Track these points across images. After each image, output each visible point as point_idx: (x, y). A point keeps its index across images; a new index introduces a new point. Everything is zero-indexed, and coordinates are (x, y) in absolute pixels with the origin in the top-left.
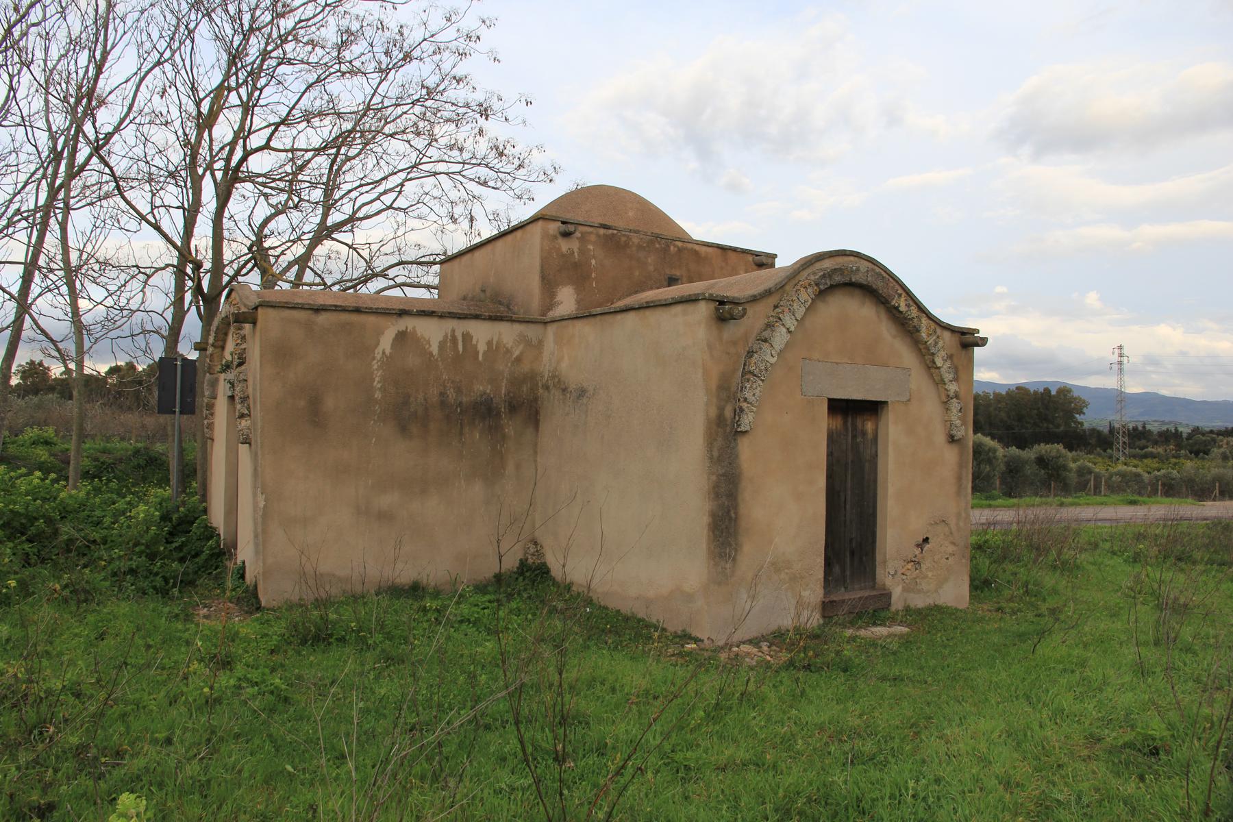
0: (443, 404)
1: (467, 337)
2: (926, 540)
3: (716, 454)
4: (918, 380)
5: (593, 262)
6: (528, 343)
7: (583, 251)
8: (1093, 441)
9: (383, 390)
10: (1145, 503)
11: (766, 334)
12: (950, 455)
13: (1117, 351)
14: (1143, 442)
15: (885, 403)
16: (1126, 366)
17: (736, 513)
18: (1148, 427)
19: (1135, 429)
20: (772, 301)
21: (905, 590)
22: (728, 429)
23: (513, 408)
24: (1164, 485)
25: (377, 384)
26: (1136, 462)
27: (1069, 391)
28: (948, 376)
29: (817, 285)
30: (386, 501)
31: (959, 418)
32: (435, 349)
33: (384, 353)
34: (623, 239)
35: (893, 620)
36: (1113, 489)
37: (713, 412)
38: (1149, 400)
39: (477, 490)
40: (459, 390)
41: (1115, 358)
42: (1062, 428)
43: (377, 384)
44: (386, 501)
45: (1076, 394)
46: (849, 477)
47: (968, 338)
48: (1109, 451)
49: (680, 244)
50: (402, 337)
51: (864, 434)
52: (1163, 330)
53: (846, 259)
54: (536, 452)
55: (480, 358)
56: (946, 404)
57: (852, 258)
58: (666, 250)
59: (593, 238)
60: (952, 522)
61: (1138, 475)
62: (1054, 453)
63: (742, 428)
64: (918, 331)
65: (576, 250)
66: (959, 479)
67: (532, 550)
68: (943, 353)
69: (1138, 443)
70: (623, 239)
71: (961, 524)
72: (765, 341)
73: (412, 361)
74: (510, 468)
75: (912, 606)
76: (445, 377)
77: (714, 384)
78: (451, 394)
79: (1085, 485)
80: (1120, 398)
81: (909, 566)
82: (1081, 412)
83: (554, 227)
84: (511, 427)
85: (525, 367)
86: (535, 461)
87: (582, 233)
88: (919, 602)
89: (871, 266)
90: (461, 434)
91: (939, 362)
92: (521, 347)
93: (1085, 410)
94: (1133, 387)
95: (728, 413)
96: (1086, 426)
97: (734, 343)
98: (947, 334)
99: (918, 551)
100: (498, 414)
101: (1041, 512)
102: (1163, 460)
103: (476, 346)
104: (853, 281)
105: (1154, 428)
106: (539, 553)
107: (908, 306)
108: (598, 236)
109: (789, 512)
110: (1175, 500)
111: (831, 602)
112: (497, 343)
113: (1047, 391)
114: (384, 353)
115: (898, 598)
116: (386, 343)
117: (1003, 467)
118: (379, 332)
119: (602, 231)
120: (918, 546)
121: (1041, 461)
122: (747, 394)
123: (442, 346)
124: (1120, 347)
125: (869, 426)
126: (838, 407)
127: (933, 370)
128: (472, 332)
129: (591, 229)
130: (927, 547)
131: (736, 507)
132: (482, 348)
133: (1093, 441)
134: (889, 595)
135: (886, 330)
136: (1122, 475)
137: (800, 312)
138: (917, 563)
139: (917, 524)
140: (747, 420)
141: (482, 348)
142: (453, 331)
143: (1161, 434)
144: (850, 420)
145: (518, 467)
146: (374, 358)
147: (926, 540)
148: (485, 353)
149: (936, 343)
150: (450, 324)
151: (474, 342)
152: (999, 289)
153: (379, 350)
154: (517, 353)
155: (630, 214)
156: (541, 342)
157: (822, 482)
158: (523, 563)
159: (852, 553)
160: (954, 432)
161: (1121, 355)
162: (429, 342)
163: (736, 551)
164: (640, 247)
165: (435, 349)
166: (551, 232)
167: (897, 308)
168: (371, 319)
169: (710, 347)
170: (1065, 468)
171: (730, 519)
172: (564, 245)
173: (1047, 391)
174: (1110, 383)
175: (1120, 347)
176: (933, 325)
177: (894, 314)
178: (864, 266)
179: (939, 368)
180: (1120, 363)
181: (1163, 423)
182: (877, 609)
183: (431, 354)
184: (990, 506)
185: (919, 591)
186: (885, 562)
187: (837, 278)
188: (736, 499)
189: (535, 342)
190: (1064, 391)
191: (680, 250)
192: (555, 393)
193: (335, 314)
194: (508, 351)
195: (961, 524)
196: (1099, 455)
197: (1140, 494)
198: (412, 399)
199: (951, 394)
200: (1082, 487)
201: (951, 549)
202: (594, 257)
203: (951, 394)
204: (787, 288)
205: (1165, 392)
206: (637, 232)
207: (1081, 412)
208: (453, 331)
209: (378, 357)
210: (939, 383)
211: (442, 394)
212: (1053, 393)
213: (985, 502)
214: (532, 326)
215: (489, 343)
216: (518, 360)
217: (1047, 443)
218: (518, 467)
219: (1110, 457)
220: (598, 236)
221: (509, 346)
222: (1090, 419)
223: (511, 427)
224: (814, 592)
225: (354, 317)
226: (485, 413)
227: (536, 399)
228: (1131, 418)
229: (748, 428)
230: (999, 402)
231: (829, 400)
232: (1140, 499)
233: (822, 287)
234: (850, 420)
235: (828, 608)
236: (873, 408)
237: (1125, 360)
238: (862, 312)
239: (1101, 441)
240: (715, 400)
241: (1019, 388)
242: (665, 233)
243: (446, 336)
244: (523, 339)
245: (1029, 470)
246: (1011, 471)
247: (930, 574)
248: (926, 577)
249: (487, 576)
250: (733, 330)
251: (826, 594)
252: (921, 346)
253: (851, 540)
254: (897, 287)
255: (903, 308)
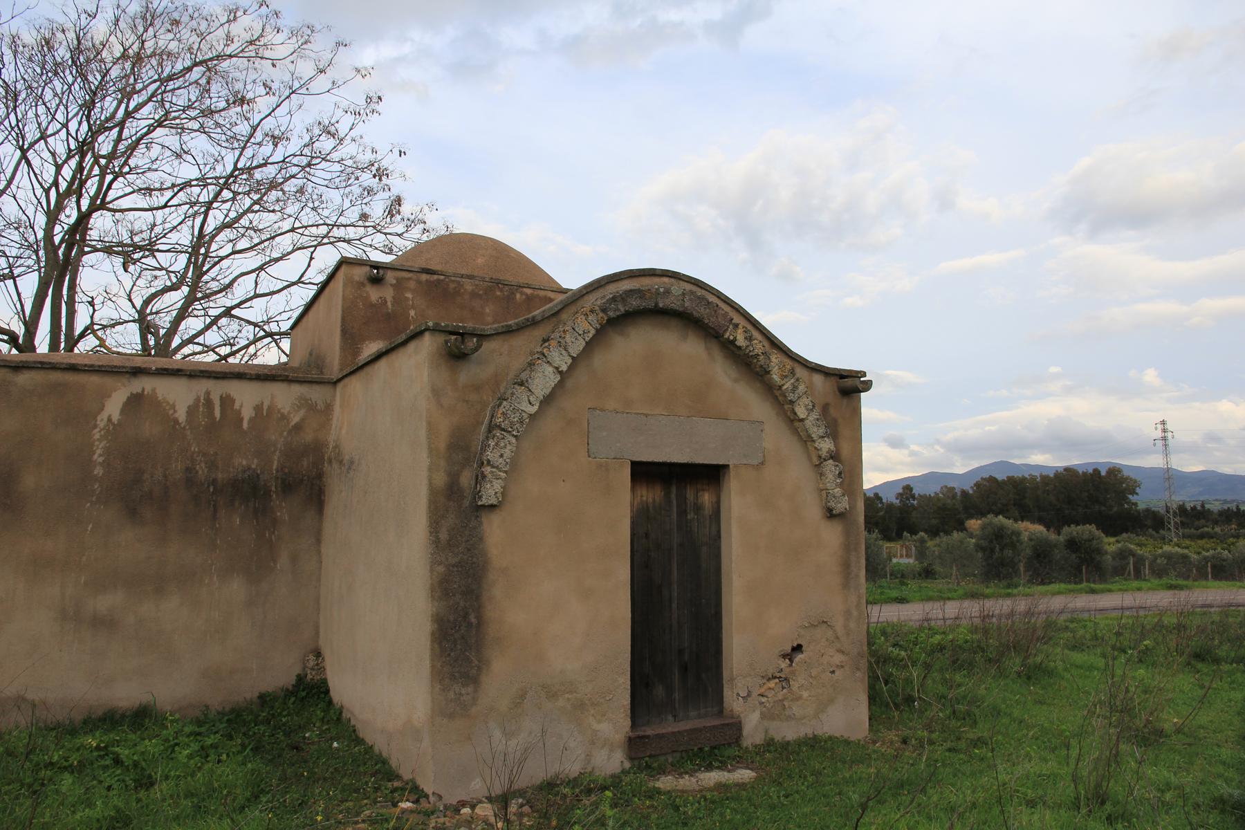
0: (189, 480)
1: (227, 401)
2: (798, 648)
3: (444, 536)
4: (775, 436)
5: (412, 313)
6: (312, 408)
7: (396, 300)
8: (1149, 522)
9: (106, 464)
10: (1187, 587)
11: (524, 376)
12: (832, 535)
13: (1160, 427)
14: (1203, 522)
15: (726, 467)
16: (1170, 441)
17: (479, 618)
18: (1207, 506)
19: (1194, 508)
20: (539, 333)
21: (763, 716)
22: (466, 503)
23: (288, 485)
24: (1213, 567)
25: (98, 457)
26: (1188, 542)
27: (1119, 471)
28: (816, 431)
29: (604, 310)
30: (104, 603)
31: (841, 485)
32: (181, 415)
33: (109, 420)
34: (452, 286)
35: (742, 760)
36: (1159, 573)
37: (441, 479)
38: (1207, 479)
39: (236, 588)
40: (212, 465)
41: (1159, 434)
42: (1115, 509)
43: (98, 457)
44: (104, 603)
45: (1126, 473)
46: (675, 566)
47: (848, 382)
48: (1162, 532)
49: (529, 291)
50: (135, 402)
51: (698, 508)
52: (1225, 406)
53: (657, 280)
54: (319, 541)
55: (245, 425)
56: (818, 467)
57: (666, 280)
58: (510, 298)
59: (412, 285)
60: (839, 623)
61: (1185, 557)
62: (1086, 537)
63: (484, 501)
64: (768, 372)
65: (389, 299)
66: (846, 566)
67: (311, 663)
68: (805, 401)
69: (1196, 523)
70: (452, 286)
71: (852, 625)
72: (521, 384)
73: (149, 429)
74: (283, 561)
75: (778, 738)
76: (194, 448)
77: (442, 445)
78: (202, 470)
79: (1128, 569)
80: (1169, 477)
81: (772, 684)
82: (1134, 493)
83: (360, 273)
84: (283, 509)
85: (308, 436)
86: (319, 552)
87: (398, 279)
88: (788, 732)
89: (688, 287)
90: (214, 517)
91: (801, 412)
92: (302, 413)
93: (1138, 490)
94: (1190, 465)
95: (466, 479)
96: (1141, 506)
97: (477, 388)
98: (818, 379)
99: (784, 664)
100: (268, 493)
101: (1128, 599)
102: (1221, 539)
103: (239, 412)
104: (660, 306)
105: (1215, 507)
106: (320, 668)
107: (750, 339)
108: (419, 282)
109: (570, 612)
110: (1223, 583)
111: (639, 737)
112: (269, 407)
113: (1096, 472)
114: (109, 420)
115: (753, 728)
116: (113, 408)
117: (1029, 552)
118: (105, 395)
119: (424, 277)
120: (784, 656)
121: (1072, 544)
122: (490, 455)
123: (191, 411)
124: (1163, 423)
125: (706, 498)
126: (643, 472)
127: (797, 424)
128: (234, 394)
129: (410, 275)
130: (799, 657)
131: (479, 611)
132: (247, 413)
133: (1149, 522)
134: (737, 726)
135: (722, 373)
136: (1169, 557)
137: (577, 347)
138: (785, 681)
139: (782, 627)
140: (490, 493)
141: (247, 413)
142: (208, 393)
143: (1221, 513)
144: (674, 490)
145: (294, 559)
146: (95, 426)
147: (798, 648)
148: (251, 420)
149: (795, 388)
150: (204, 385)
151: (237, 406)
152: (1053, 369)
153: (104, 416)
154: (295, 419)
155: (479, 261)
156: (329, 407)
157: (623, 573)
158: (300, 679)
159: (684, 669)
160: (832, 504)
161: (1164, 431)
162: (173, 407)
163: (479, 668)
164: (474, 295)
165: (181, 415)
166: (357, 278)
167: (733, 342)
168: (95, 379)
169: (436, 393)
170: (1099, 551)
171: (470, 624)
172: (374, 294)
173: (1096, 472)
174: (1154, 461)
175: (1163, 423)
176: (789, 364)
177: (731, 350)
178: (677, 288)
179: (802, 420)
180: (1164, 439)
181: (1225, 502)
182: (722, 744)
183: (176, 421)
184: (1009, 595)
185: (789, 718)
186: (732, 679)
187: (635, 303)
188: (478, 597)
189: (321, 406)
190: (1114, 471)
191: (529, 298)
192: (335, 465)
193: (42, 372)
194: (283, 417)
195: (852, 625)
196: (1151, 536)
197: (1187, 578)
198: (146, 476)
199: (824, 454)
200: (1120, 571)
201: (838, 659)
202: (413, 307)
203: (824, 454)
204: (564, 316)
205: (1227, 470)
206: (471, 277)
207: (1134, 493)
208: (208, 393)
209: (102, 425)
210: (806, 440)
211: (188, 470)
212: (1103, 473)
213: (1003, 591)
214: (316, 388)
215: (258, 408)
216: (298, 428)
217: (1078, 524)
218: (294, 559)
219: (1164, 538)
220: (419, 282)
221: (285, 411)
222: (1143, 500)
223: (283, 509)
224: (614, 723)
225: (70, 377)
226: (249, 493)
227: (320, 476)
228: (1187, 497)
229: (493, 501)
230: (1047, 484)
231: (634, 464)
232: (1185, 583)
233: (611, 314)
234: (674, 490)
235: (635, 745)
236: (713, 474)
237: (1169, 435)
238: (684, 352)
239: (1152, 522)
240: (443, 463)
241: (1067, 469)
242: (508, 277)
243: (198, 400)
244: (305, 403)
245: (1058, 554)
246: (1039, 556)
247: (805, 694)
248: (800, 698)
249: (248, 696)
250: (469, 373)
251: (634, 725)
252: (777, 393)
253: (681, 652)
254: (732, 314)
255: (741, 341)
